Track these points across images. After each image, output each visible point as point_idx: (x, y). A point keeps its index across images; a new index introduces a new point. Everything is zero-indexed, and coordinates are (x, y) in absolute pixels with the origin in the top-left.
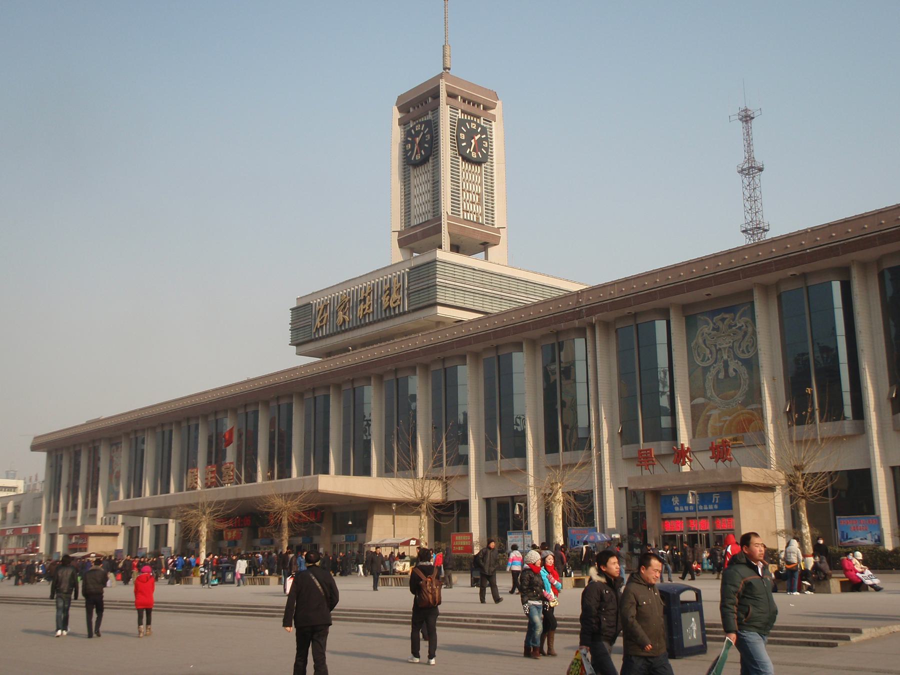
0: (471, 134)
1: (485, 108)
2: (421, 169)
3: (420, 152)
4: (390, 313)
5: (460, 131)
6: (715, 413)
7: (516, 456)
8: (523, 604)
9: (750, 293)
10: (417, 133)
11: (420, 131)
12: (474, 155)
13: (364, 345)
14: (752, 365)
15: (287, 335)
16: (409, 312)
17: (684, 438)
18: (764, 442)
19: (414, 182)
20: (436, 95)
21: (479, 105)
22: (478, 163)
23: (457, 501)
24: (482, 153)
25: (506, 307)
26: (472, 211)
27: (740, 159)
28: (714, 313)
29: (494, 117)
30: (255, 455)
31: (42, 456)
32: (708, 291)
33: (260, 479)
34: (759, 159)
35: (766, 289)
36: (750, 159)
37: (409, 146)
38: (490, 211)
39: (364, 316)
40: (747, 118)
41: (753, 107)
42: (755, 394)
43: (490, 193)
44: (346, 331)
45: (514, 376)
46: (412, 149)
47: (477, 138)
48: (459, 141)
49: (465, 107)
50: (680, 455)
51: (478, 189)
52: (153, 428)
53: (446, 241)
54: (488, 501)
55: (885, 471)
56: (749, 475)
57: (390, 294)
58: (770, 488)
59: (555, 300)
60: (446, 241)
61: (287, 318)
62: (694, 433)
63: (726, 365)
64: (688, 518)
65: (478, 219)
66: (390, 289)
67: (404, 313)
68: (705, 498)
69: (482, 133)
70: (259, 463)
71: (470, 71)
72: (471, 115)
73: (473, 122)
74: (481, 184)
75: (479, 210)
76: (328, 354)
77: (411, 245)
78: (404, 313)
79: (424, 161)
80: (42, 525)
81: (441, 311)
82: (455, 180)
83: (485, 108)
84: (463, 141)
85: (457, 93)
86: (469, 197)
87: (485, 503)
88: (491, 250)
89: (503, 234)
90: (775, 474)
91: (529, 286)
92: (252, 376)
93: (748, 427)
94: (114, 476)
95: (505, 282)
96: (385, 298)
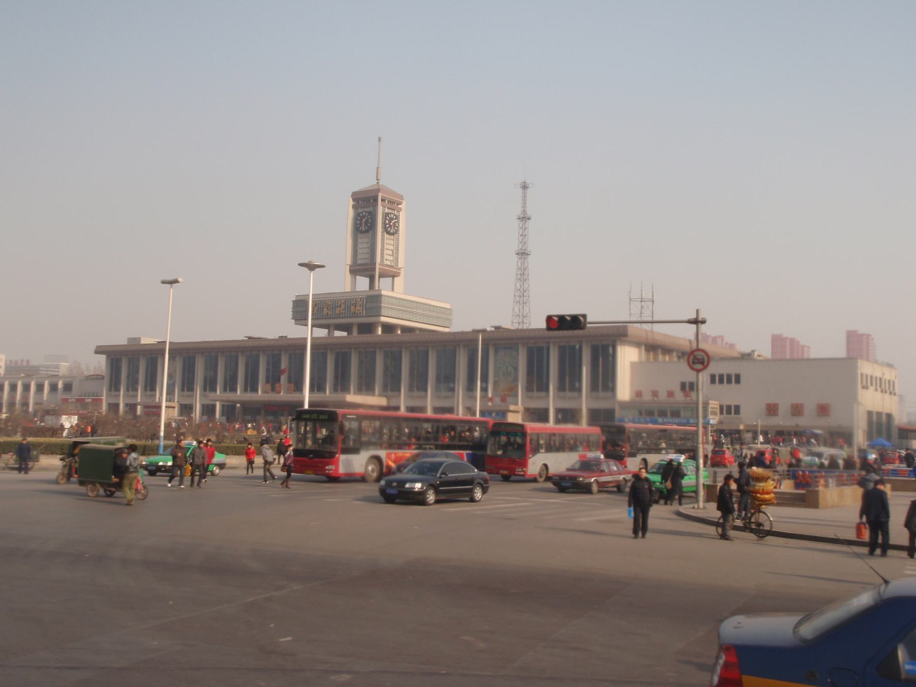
14: (516, 369)
15: (290, 314)
20: (376, 200)
22: (393, 234)
26: (389, 260)
27: (518, 211)
29: (401, 209)
31: (103, 358)
34: (529, 212)
36: (524, 212)
40: (525, 187)
41: (528, 181)
42: (516, 379)
43: (397, 249)
46: (361, 224)
49: (389, 206)
51: (392, 248)
56: (512, 408)
61: (291, 305)
62: (494, 390)
82: (383, 245)
89: (402, 271)
90: (520, 407)
93: (513, 390)
96: (353, 308)
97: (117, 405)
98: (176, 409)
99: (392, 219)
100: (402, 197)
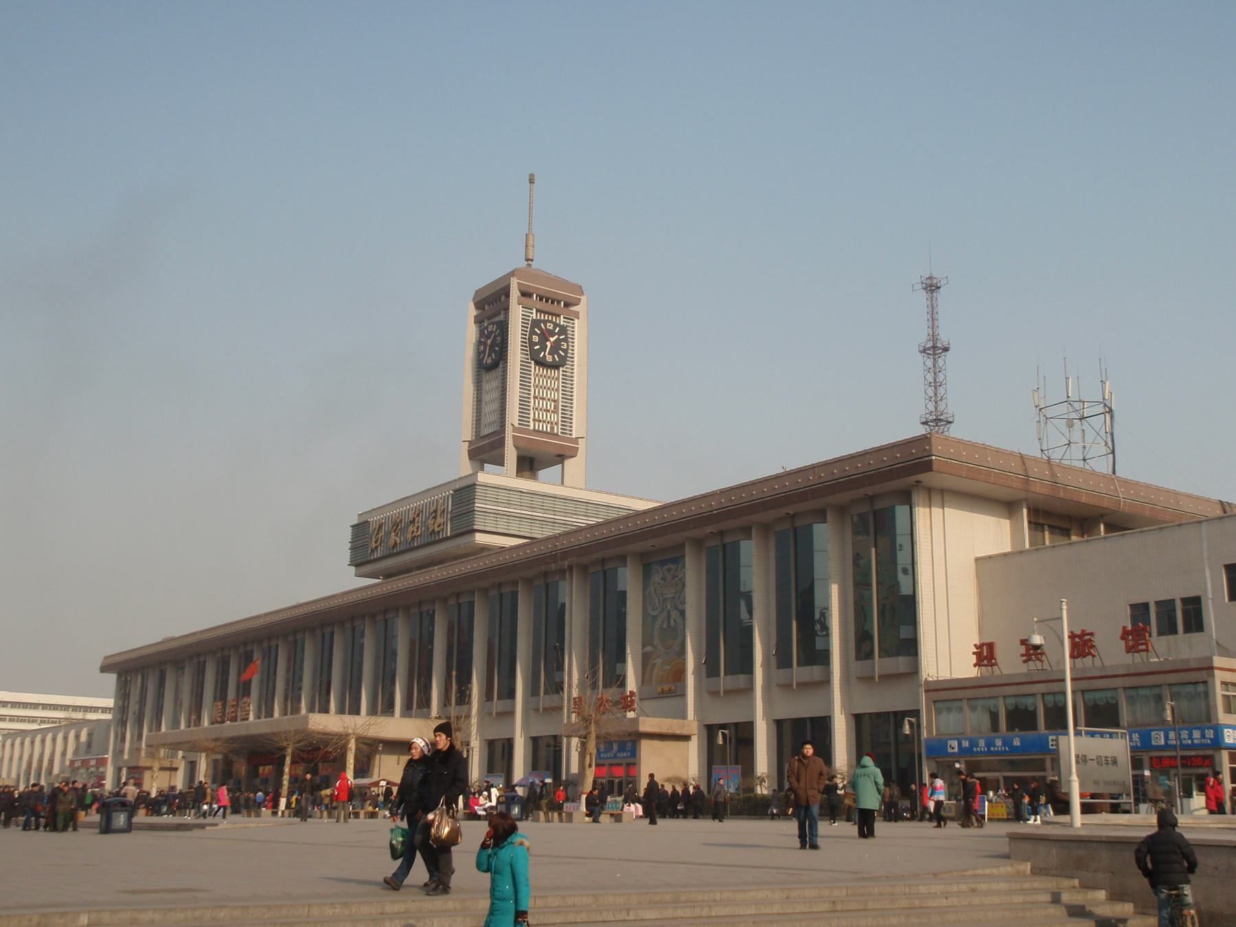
0: (544, 337)
1: (566, 305)
2: (493, 374)
3: (491, 358)
4: (434, 538)
5: (533, 333)
6: (659, 661)
7: (742, 672)
8: (1156, 894)
9: (681, 547)
10: (490, 333)
11: (492, 332)
12: (549, 359)
13: (420, 568)
15: (346, 555)
16: (452, 537)
17: (632, 684)
18: (683, 695)
19: (487, 386)
20: (506, 292)
21: (559, 302)
22: (555, 366)
23: (812, 719)
24: (559, 355)
25: (548, 532)
26: (542, 419)
27: (922, 337)
28: (663, 563)
29: (577, 315)
30: (360, 681)
32: (651, 542)
33: (276, 714)
35: (698, 543)
36: (934, 337)
37: (482, 348)
38: (567, 420)
39: (413, 538)
40: (932, 287)
43: (568, 398)
44: (398, 554)
45: (816, 554)
46: (484, 351)
47: (552, 339)
48: (532, 344)
49: (543, 305)
50: (626, 703)
51: (554, 395)
52: (313, 630)
53: (511, 455)
54: (779, 723)
55: (846, 718)
57: (435, 517)
58: (686, 738)
59: (618, 520)
60: (511, 455)
61: (347, 535)
62: (644, 680)
63: (669, 616)
64: (611, 765)
65: (552, 428)
66: (435, 511)
67: (447, 539)
68: (622, 747)
69: (559, 334)
70: (628, 650)
71: (554, 263)
72: (549, 314)
73: (551, 322)
74: (557, 390)
75: (554, 418)
76: (388, 575)
77: (482, 457)
78: (447, 539)
79: (494, 366)
80: (109, 756)
81: (480, 538)
82: (524, 384)
83: (566, 305)
84: (536, 344)
85: (531, 291)
86: (543, 404)
87: (705, 732)
88: (567, 463)
89: (582, 445)
90: (691, 722)
91: (590, 507)
92: (792, 466)
94: (177, 702)
95: (559, 505)
97: (509, 744)
98: (695, 739)
99: (552, 333)
100: (580, 290)
